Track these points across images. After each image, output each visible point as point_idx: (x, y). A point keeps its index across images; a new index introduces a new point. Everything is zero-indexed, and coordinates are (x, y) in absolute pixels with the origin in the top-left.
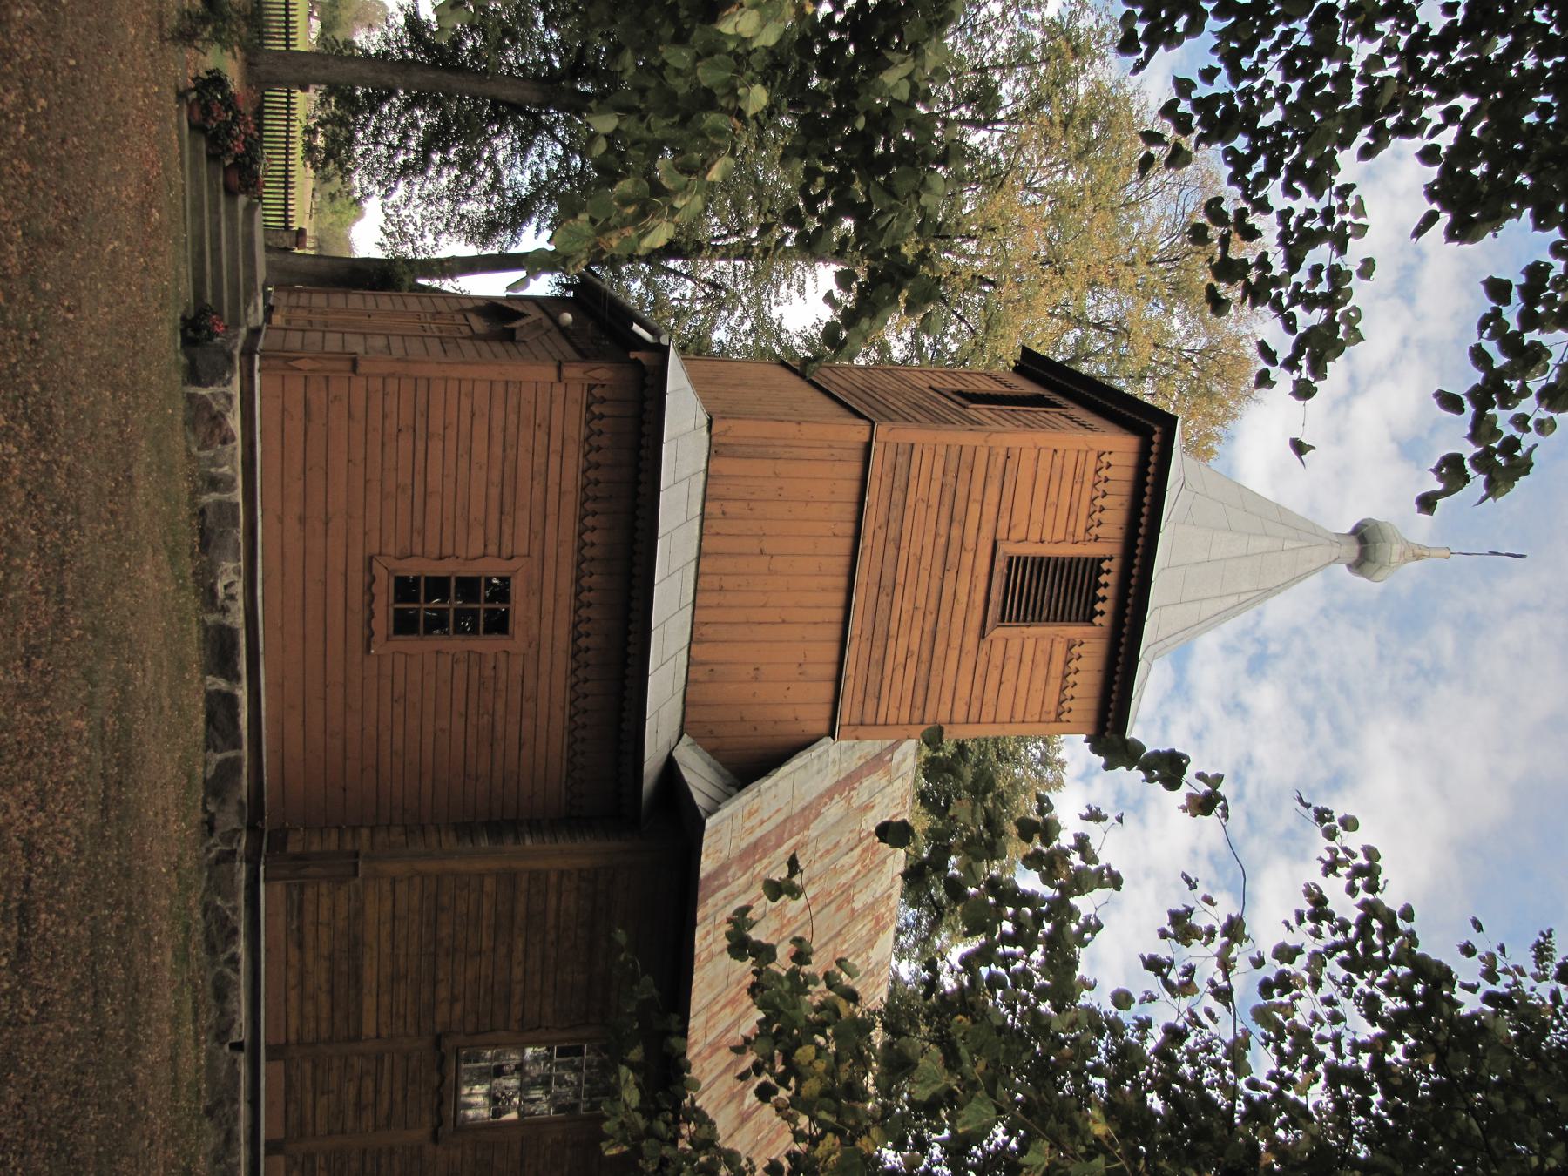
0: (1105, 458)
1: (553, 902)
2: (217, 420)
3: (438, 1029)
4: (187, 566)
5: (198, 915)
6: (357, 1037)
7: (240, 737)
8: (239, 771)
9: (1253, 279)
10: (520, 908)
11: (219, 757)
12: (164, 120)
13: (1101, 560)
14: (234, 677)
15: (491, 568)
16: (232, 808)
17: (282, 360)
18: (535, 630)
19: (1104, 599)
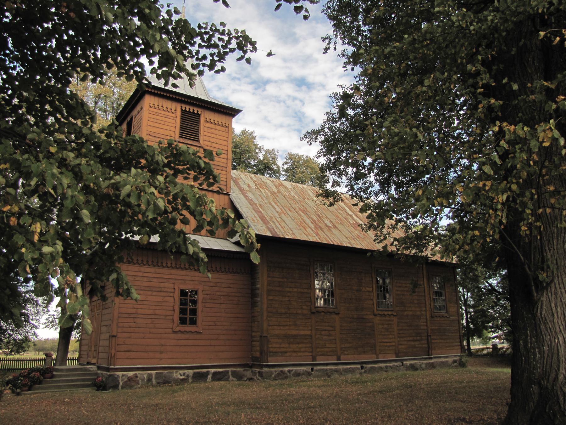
0: (152, 105)
1: (276, 279)
2: (130, 379)
3: (310, 313)
4: (175, 387)
5: (277, 382)
6: (311, 336)
7: (225, 371)
8: (235, 371)
9: (217, 59)
10: (278, 289)
11: (231, 377)
12: (31, 399)
13: (182, 110)
14: (208, 373)
15: (177, 294)
16: (245, 373)
17: (111, 358)
18: (196, 282)
19: (193, 110)
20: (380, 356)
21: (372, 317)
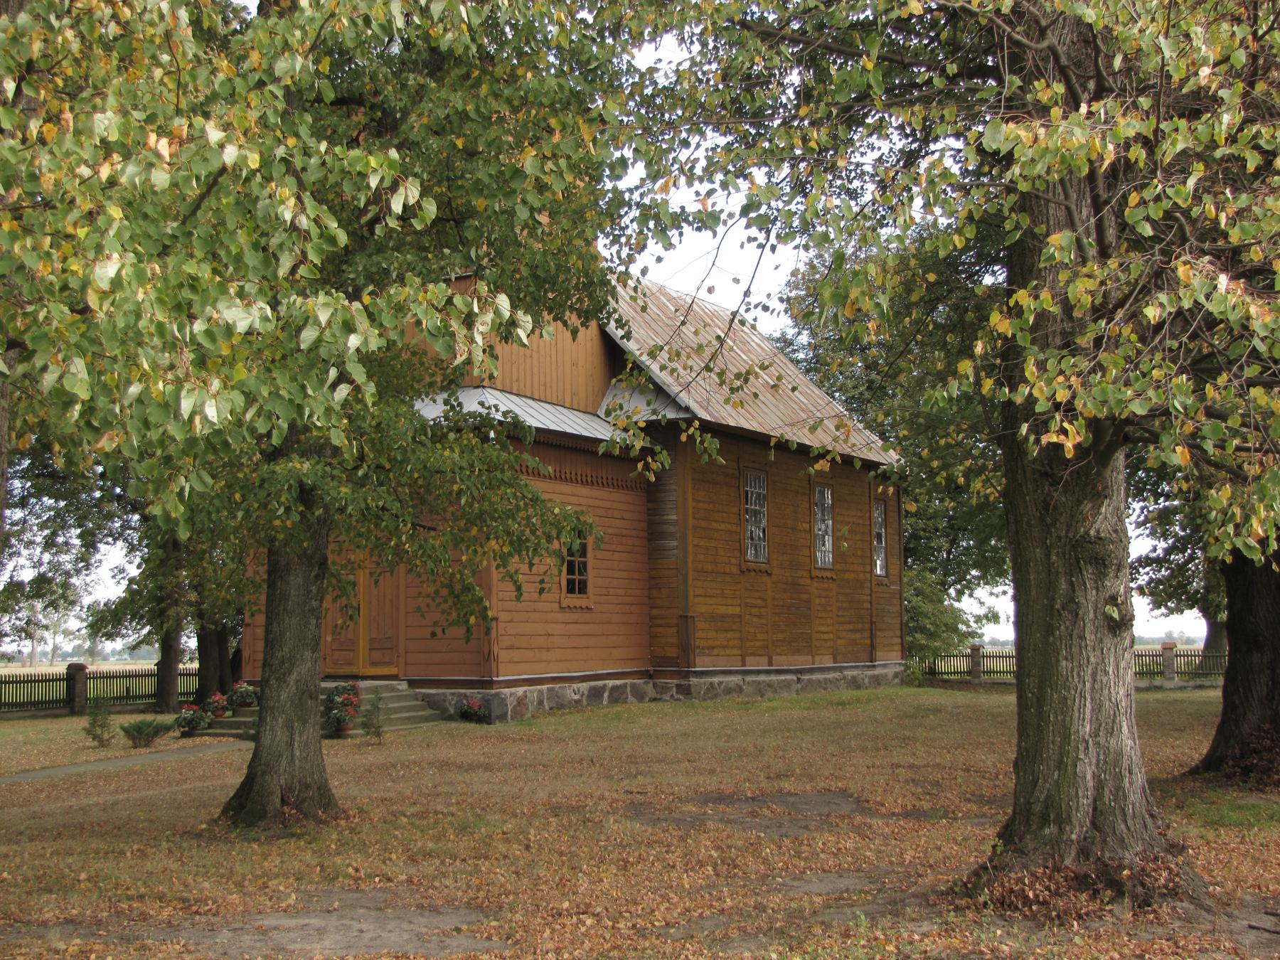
6: (740, 616)
20: (817, 658)
21: (808, 581)
